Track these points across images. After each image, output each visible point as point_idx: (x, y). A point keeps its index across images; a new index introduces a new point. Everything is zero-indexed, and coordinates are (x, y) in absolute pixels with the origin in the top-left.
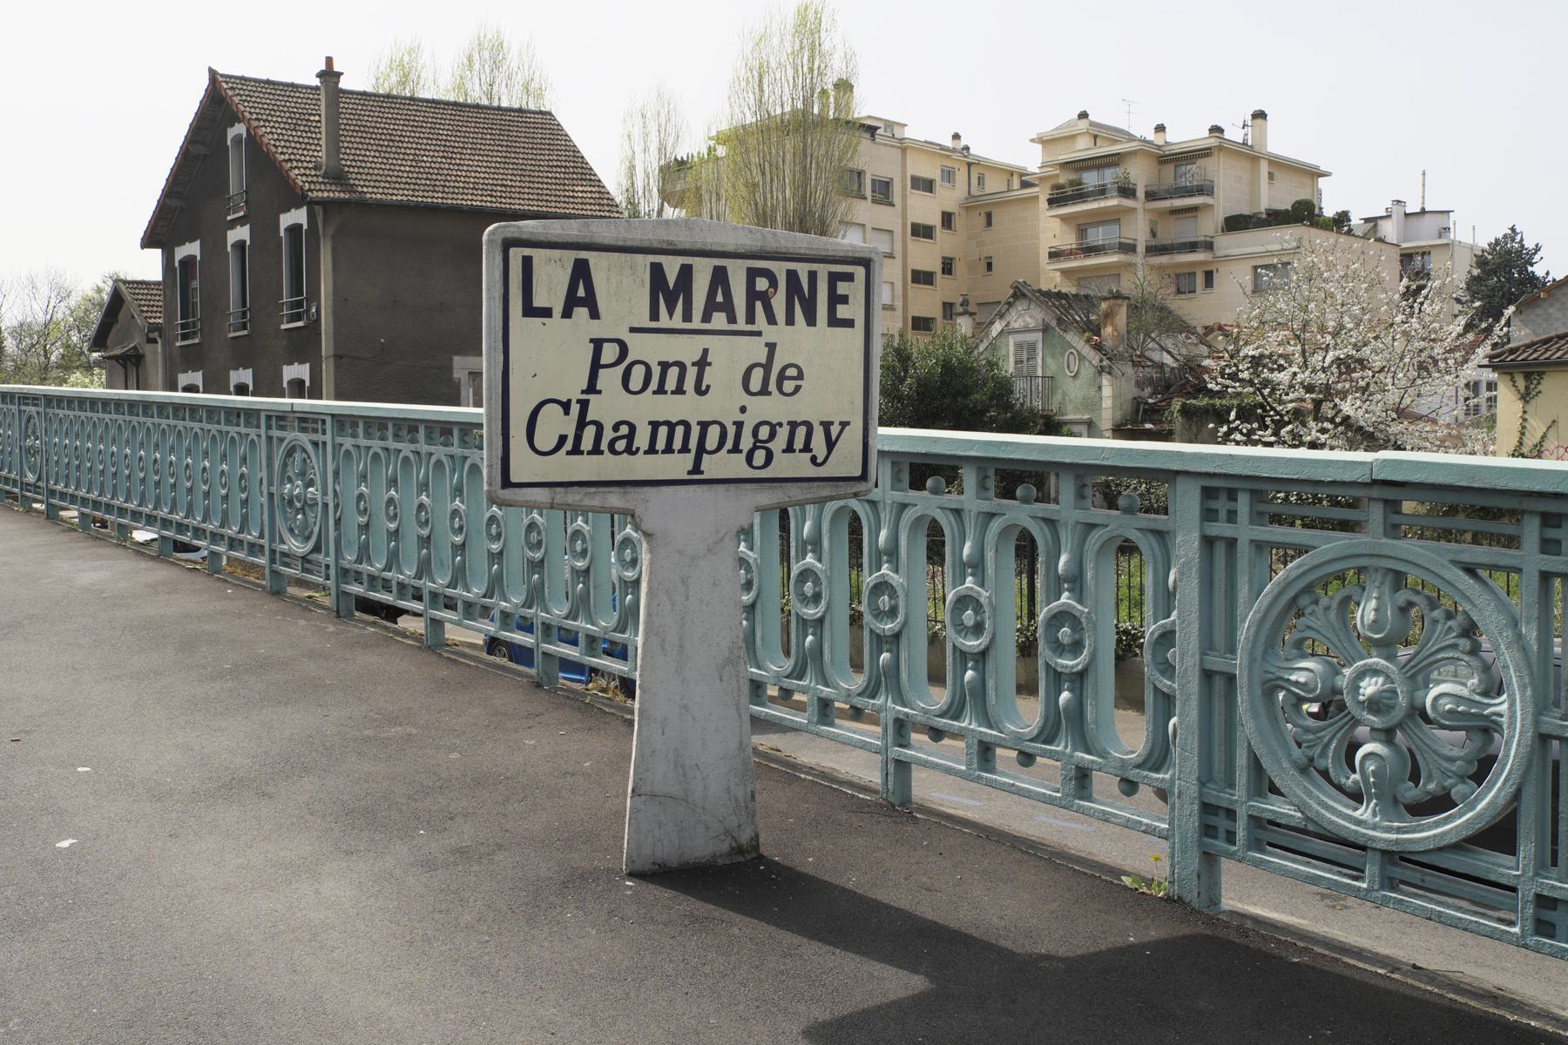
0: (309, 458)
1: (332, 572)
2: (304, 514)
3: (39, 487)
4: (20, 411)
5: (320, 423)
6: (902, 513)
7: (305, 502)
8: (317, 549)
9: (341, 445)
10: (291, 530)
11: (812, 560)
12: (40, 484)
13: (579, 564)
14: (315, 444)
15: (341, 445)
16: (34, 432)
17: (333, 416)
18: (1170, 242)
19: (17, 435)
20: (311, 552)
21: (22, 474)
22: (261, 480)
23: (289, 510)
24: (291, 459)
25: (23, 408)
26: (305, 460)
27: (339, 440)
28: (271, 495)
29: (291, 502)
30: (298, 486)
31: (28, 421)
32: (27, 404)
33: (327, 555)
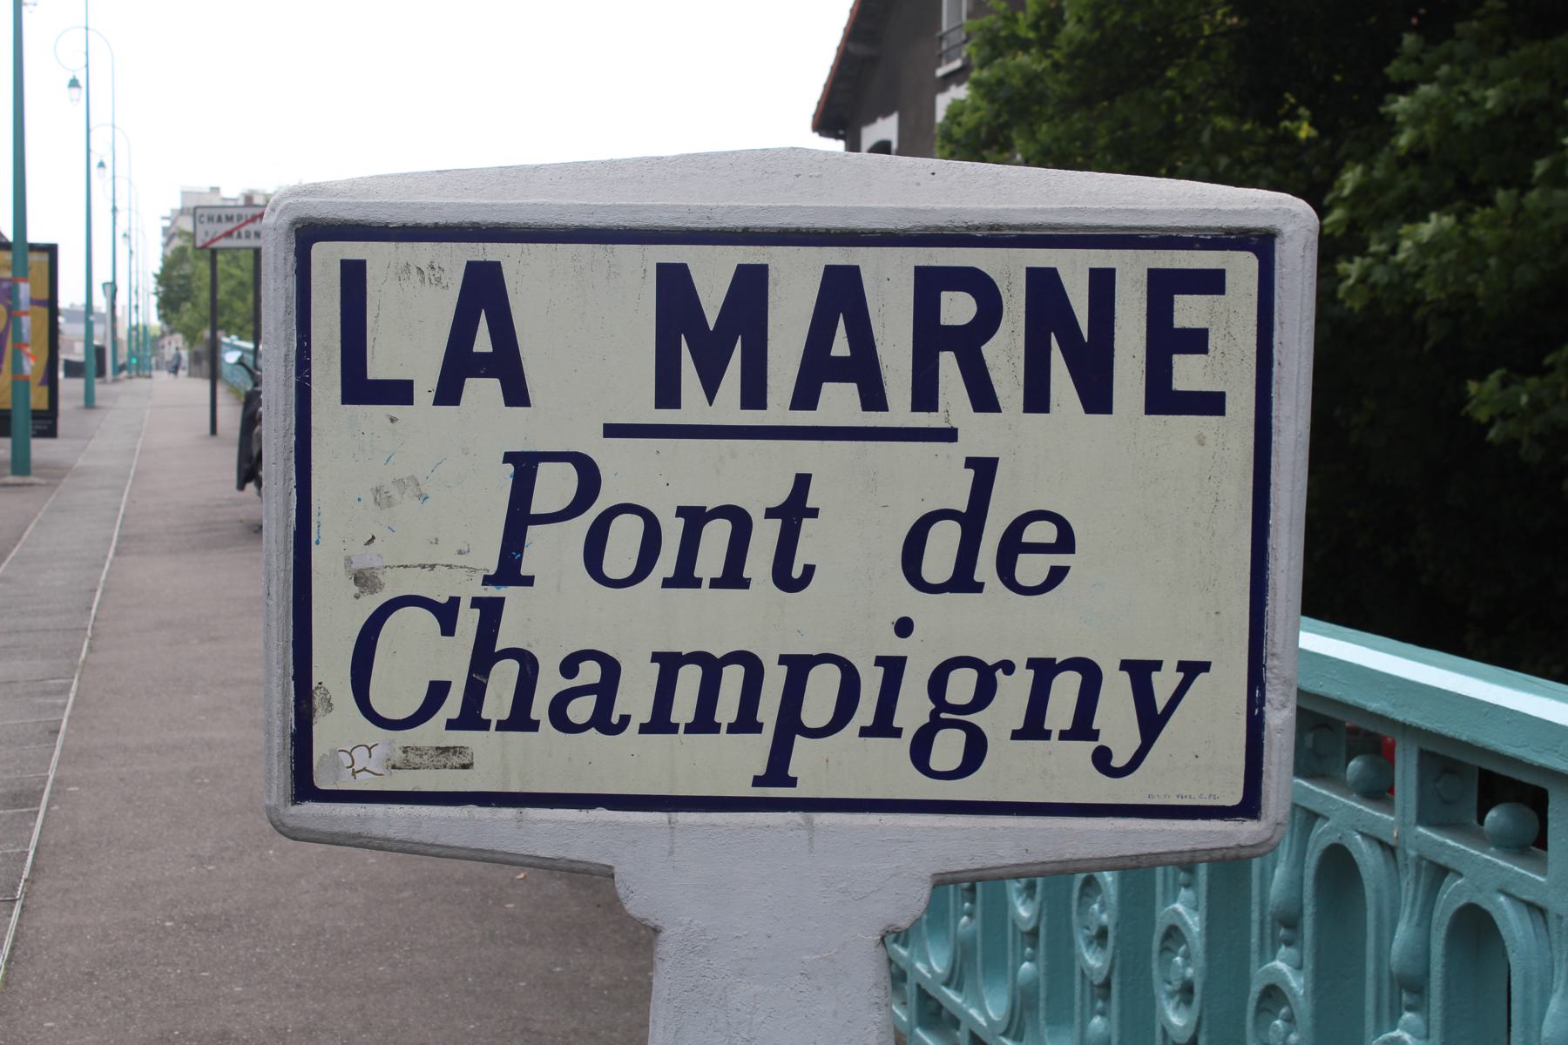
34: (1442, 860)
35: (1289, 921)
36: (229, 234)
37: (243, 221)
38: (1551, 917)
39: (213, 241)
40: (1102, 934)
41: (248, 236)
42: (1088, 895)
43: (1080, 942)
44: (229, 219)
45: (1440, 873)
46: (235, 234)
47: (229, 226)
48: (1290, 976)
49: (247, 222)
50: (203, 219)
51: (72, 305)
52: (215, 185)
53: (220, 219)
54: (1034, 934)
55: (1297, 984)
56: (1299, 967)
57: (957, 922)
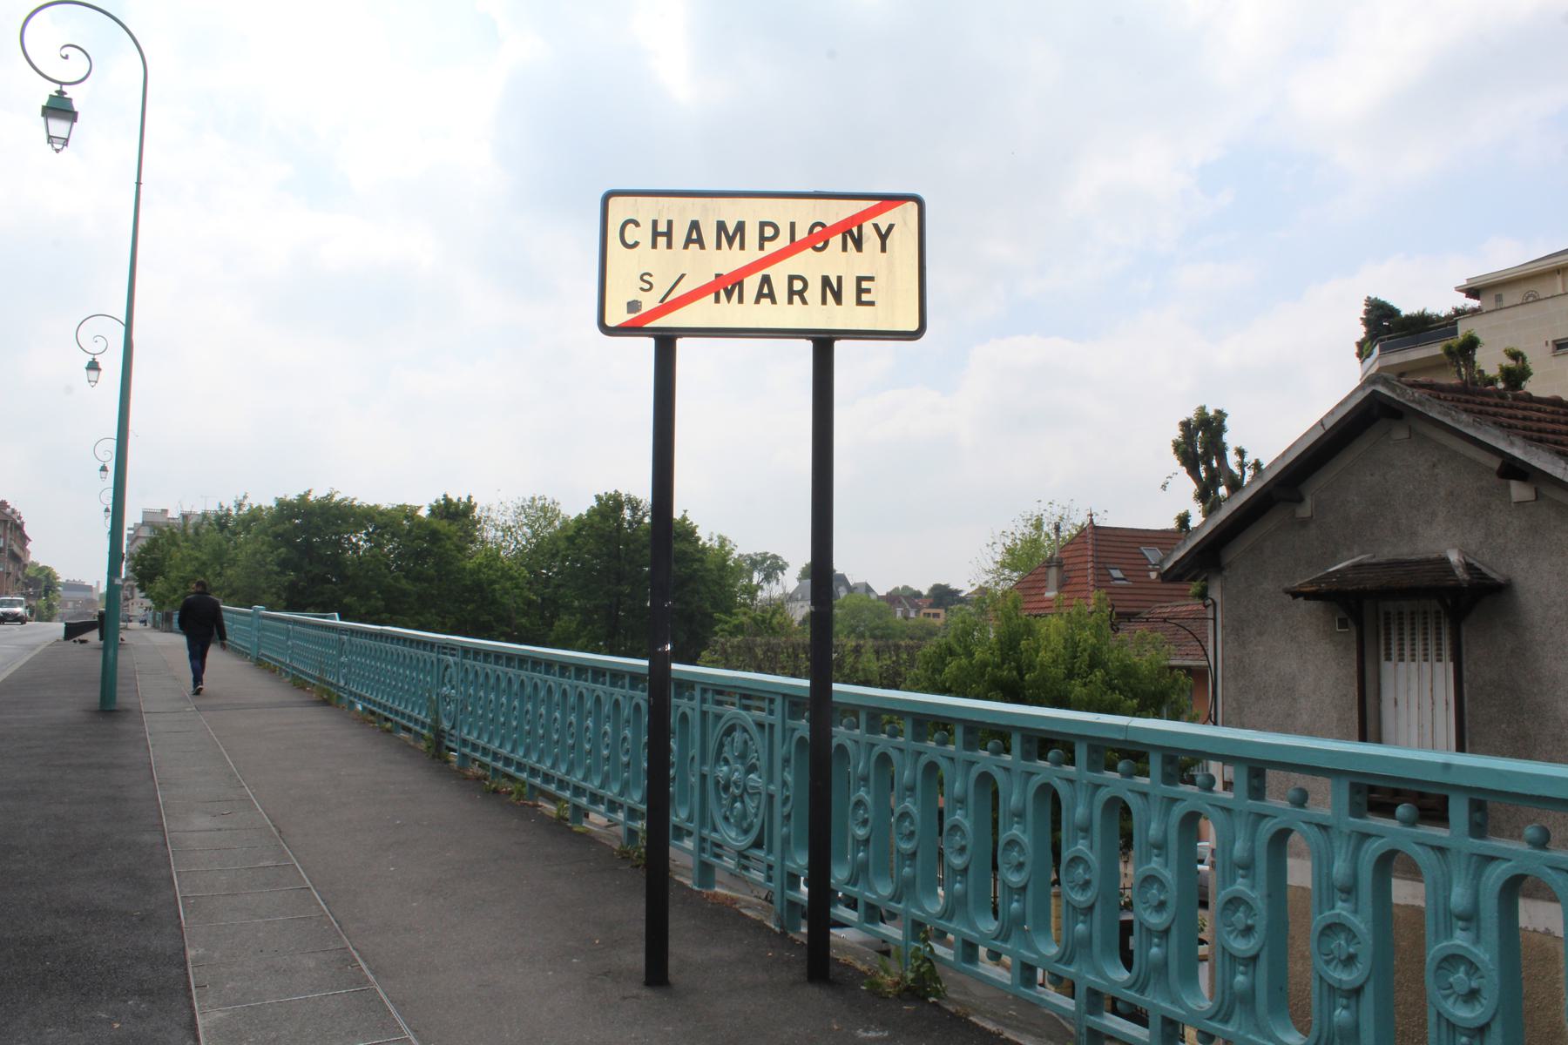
0: (752, 739)
1: (776, 873)
2: (743, 802)
3: (452, 735)
4: (438, 660)
5: (767, 701)
6: (1027, 783)
7: (745, 789)
8: (757, 844)
9: (794, 730)
10: (726, 819)
11: (1018, 833)
12: (453, 732)
13: (1014, 879)
14: (761, 726)
15: (794, 730)
16: (450, 681)
17: (784, 696)
18: (1435, 556)
19: (435, 682)
20: (750, 848)
21: (338, 681)
22: (693, 758)
23: (724, 796)
24: (729, 739)
25: (441, 656)
26: (746, 742)
27: (790, 723)
28: (703, 777)
29: (726, 788)
30: (737, 770)
31: (446, 669)
32: (445, 654)
33: (770, 851)
34: (919, 750)
35: (608, 717)
36: (728, 286)
37: (783, 241)
38: (956, 760)
39: (666, 307)
40: (608, 745)
41: (796, 293)
42: (1328, 936)
43: (621, 754)
44: (731, 235)
45: (632, 698)
46: (752, 284)
47: (730, 260)
48: (866, 797)
49: (795, 247)
50: (631, 234)
51: (67, 581)
52: (166, 508)
53: (695, 236)
54: (608, 758)
55: (868, 799)
56: (915, 804)
57: (622, 774)
